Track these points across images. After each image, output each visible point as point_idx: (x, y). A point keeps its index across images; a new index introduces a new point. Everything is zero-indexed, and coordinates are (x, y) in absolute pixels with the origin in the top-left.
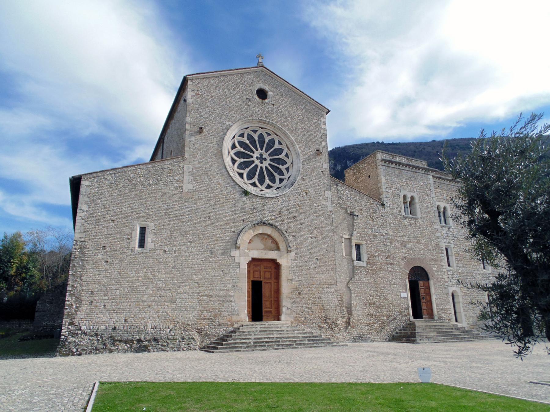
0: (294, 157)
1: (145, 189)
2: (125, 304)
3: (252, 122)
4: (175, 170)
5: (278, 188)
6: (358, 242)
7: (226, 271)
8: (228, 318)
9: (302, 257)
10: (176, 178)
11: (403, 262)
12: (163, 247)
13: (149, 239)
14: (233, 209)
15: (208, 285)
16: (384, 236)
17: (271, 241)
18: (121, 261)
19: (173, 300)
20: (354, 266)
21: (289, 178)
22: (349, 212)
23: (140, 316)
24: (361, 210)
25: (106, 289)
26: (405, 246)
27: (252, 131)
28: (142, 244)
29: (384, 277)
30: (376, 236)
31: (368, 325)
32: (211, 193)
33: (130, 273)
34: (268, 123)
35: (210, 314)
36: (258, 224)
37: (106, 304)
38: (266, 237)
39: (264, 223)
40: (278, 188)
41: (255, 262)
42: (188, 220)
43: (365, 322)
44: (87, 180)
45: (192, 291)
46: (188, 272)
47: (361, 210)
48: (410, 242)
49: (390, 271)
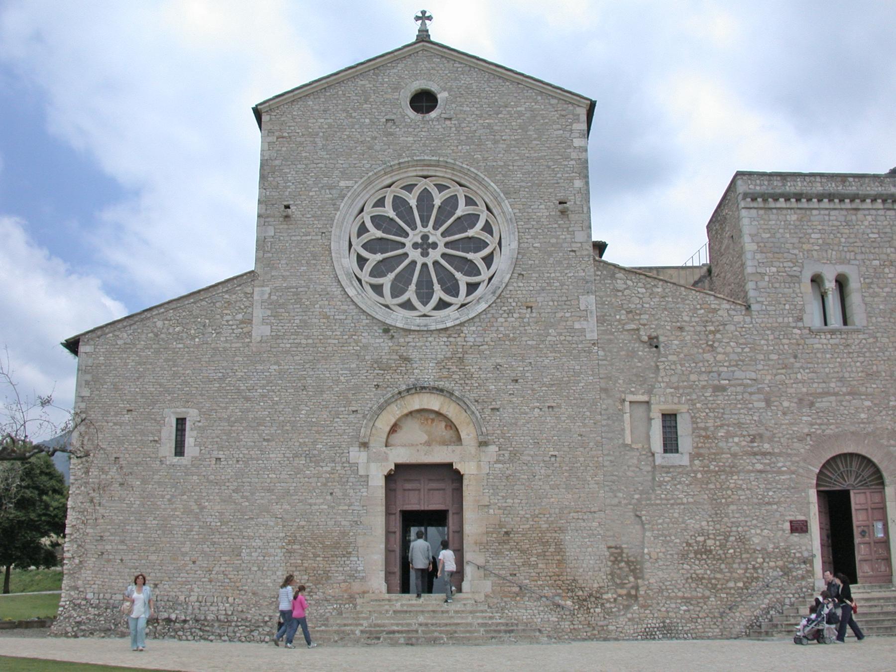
0: (504, 228)
1: (181, 346)
2: (153, 558)
3: (400, 169)
4: (235, 302)
5: (463, 305)
6: (669, 408)
7: (338, 492)
8: (343, 585)
9: (515, 455)
10: (240, 317)
11: (802, 448)
12: (215, 454)
13: (189, 441)
14: (353, 366)
15: (303, 523)
16: (746, 386)
17: (443, 424)
18: (144, 482)
19: (236, 552)
20: (654, 467)
21: (490, 279)
22: (645, 338)
23: (179, 579)
24: (681, 329)
25: (123, 531)
26: (812, 404)
27: (374, 206)
28: (180, 450)
29: (741, 488)
30: (723, 389)
31: (687, 601)
32: (307, 337)
33: (159, 503)
34: (437, 164)
35: (306, 577)
36: (408, 390)
37: (124, 557)
38: (432, 416)
39: (423, 388)
40: (463, 305)
41: (399, 475)
42: (263, 396)
43: (680, 594)
44: (87, 343)
45: (270, 535)
46: (262, 498)
47: (681, 329)
48: (827, 394)
49: (761, 472)
